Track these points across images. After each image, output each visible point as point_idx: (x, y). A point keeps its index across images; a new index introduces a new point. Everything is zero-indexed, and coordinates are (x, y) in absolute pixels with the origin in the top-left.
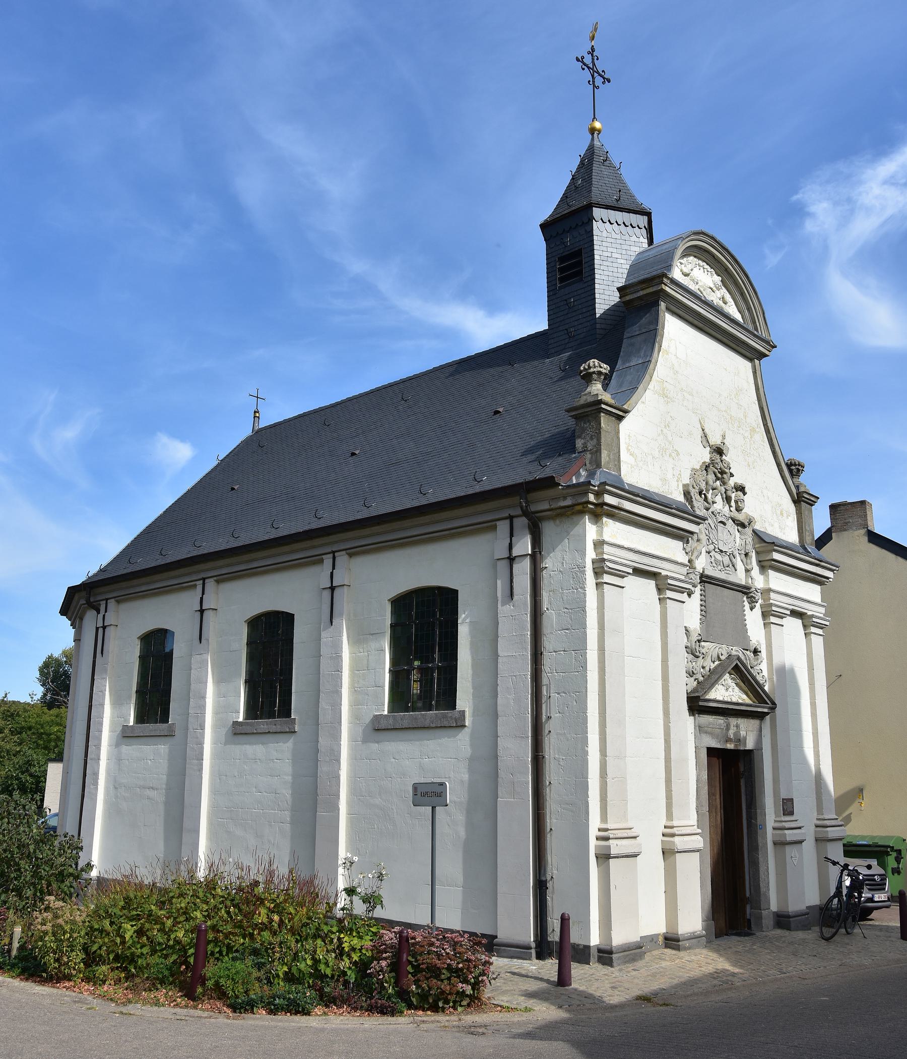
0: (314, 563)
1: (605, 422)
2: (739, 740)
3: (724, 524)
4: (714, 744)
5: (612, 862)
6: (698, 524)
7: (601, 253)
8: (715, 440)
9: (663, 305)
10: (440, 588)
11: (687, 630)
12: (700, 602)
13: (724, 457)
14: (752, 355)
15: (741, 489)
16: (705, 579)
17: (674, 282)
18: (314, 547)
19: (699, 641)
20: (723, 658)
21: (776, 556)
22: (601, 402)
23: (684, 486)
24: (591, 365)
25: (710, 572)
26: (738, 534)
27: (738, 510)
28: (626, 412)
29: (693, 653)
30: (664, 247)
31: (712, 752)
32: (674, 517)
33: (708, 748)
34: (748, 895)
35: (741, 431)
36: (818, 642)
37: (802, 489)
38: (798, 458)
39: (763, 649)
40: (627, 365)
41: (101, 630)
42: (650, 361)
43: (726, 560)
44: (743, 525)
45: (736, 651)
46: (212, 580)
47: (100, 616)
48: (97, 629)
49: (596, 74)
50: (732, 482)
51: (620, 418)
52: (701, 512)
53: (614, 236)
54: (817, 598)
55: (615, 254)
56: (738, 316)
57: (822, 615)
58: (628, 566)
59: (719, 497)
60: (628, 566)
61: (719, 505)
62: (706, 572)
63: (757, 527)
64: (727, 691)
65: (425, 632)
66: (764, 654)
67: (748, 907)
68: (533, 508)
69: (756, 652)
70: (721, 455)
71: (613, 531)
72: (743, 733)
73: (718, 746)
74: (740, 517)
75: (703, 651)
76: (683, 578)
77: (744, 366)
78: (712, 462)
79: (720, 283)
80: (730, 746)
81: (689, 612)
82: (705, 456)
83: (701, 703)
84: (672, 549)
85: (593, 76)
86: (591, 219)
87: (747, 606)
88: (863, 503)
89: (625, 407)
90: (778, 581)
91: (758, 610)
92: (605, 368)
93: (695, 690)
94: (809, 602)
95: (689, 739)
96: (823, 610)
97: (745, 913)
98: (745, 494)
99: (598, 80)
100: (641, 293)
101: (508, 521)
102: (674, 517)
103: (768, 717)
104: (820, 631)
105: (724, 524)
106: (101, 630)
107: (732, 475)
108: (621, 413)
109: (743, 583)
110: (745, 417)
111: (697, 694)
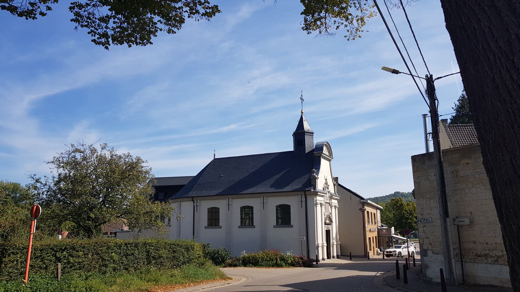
14: (330, 161)
64: (328, 221)
82: (325, 181)
90: (333, 201)
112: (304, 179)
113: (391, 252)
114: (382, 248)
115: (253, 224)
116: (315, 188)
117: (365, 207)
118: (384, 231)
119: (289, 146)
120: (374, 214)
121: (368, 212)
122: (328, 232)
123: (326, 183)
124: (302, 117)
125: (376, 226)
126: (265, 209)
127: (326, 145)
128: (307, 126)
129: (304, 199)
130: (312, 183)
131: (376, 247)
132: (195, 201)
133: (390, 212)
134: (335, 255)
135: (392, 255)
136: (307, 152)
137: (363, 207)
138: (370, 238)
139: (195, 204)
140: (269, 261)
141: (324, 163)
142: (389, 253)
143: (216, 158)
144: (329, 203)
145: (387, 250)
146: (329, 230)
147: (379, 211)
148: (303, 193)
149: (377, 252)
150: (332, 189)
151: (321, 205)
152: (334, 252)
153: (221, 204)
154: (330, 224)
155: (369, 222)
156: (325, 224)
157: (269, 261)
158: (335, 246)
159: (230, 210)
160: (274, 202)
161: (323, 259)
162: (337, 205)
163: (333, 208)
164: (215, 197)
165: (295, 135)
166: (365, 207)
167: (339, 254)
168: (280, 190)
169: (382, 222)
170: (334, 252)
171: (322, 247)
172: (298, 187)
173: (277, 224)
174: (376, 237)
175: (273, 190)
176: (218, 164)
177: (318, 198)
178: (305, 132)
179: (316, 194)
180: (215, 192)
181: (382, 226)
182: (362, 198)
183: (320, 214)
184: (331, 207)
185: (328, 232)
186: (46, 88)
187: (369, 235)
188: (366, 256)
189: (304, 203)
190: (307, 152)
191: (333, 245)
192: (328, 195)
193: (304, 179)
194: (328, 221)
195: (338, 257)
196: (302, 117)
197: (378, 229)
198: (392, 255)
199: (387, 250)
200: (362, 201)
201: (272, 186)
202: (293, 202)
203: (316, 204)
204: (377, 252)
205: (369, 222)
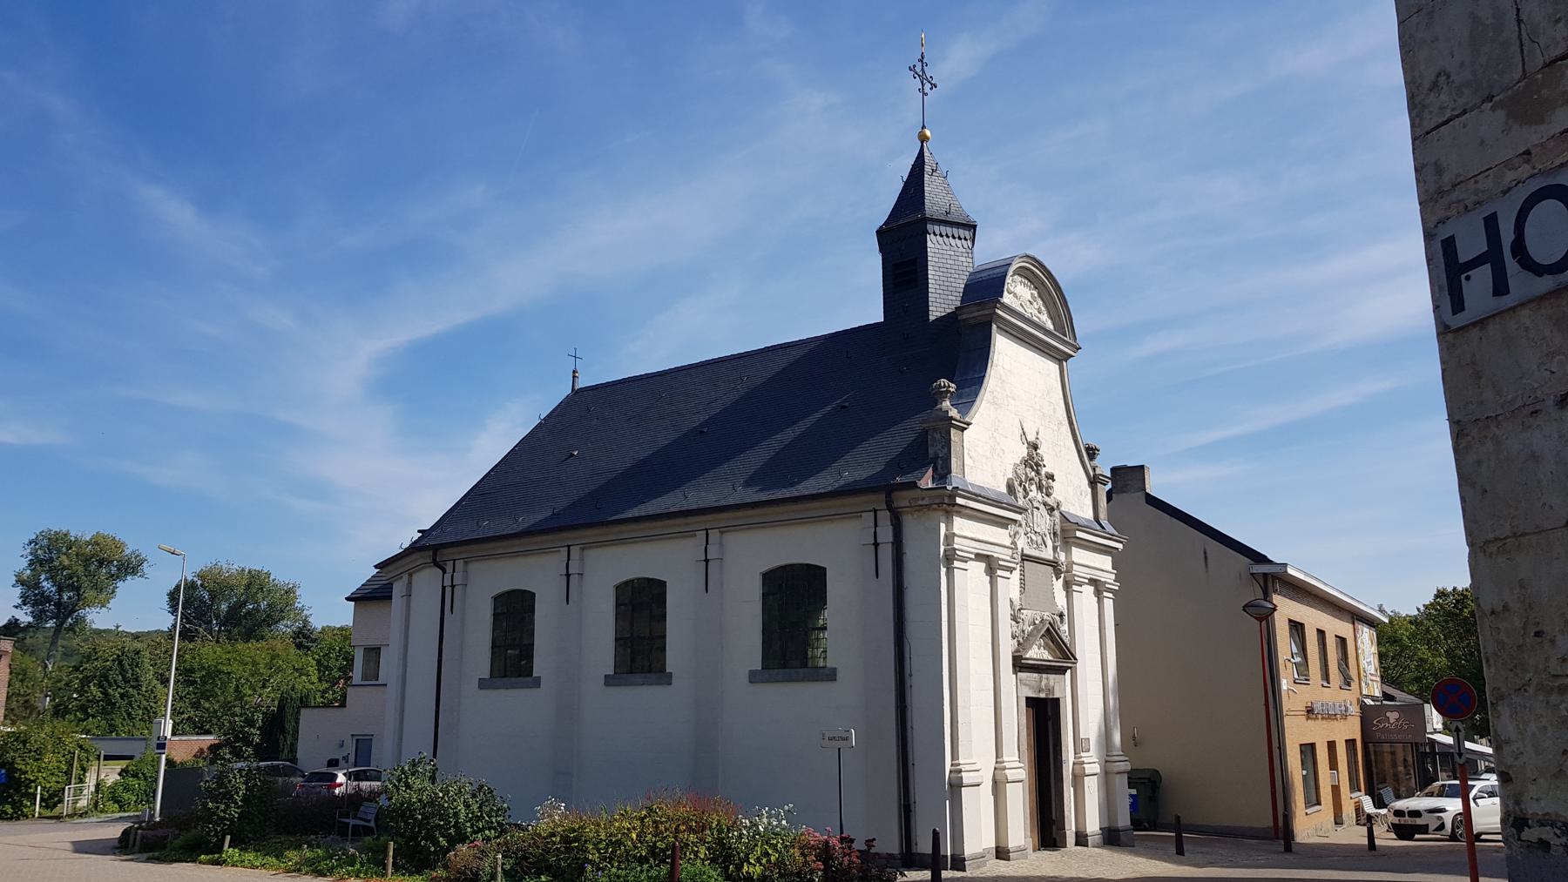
2: (1050, 690)
8: (1031, 438)
10: (808, 565)
14: (1061, 358)
15: (1051, 477)
16: (1025, 558)
17: (1105, 550)
21: (1079, 534)
27: (1048, 495)
29: (1015, 619)
32: (1002, 509)
36: (1109, 605)
37: (1098, 471)
38: (1093, 444)
41: (448, 590)
44: (1052, 509)
48: (444, 588)
55: (947, 272)
56: (1050, 325)
61: (1034, 493)
63: (1054, 484)
64: (1038, 652)
65: (794, 599)
69: (1061, 616)
74: (1050, 501)
77: (1053, 367)
78: (1030, 457)
80: (1042, 695)
81: (1010, 587)
82: (1023, 451)
84: (1001, 535)
90: (1078, 555)
99: (918, 69)
102: (1002, 509)
106: (448, 590)
112: (895, 440)
113: (1416, 814)
114: (1387, 793)
115: (663, 669)
117: (1277, 599)
118: (1393, 716)
119: (863, 305)
120: (1342, 641)
121: (1321, 633)
122: (1044, 718)
123: (1033, 461)
125: (1349, 698)
126: (716, 586)
127: (1022, 272)
128: (935, 196)
129: (886, 534)
130: (932, 449)
131: (1354, 787)
133: (1432, 643)
134: (1093, 825)
135: (1424, 829)
136: (932, 318)
137: (1267, 597)
138: (1308, 750)
139: (447, 583)
142: (1407, 820)
144: (1054, 565)
145: (1401, 804)
146: (1056, 702)
147: (1366, 636)
148: (879, 500)
149: (1359, 809)
150: (1074, 494)
151: (992, 566)
152: (1087, 807)
153: (536, 573)
154: (1062, 671)
155: (1302, 669)
156: (1020, 665)
157: (642, 860)
158: (1092, 787)
161: (1002, 853)
162: (1109, 578)
164: (517, 545)
165: (886, 236)
166: (1277, 599)
167: (1124, 820)
169: (1386, 678)
170: (1087, 807)
171: (998, 786)
172: (861, 474)
174: (1350, 743)
175: (752, 495)
176: (587, 411)
177: (961, 525)
178: (926, 220)
179: (947, 503)
180: (524, 522)
181: (1387, 696)
182: (1261, 559)
183: (976, 620)
184: (1067, 586)
185: (1044, 718)
186: (415, 318)
187: (1297, 732)
188: (1282, 832)
189: (886, 553)
190: (932, 318)
191: (1078, 779)
192: (1043, 522)
193: (895, 440)
194: (1038, 652)
195: (1112, 838)
197: (1363, 706)
198: (1424, 829)
199: (1401, 804)
200: (1261, 569)
201: (748, 483)
202: (836, 547)
203: (951, 557)
204: (1359, 809)
205: (1302, 669)
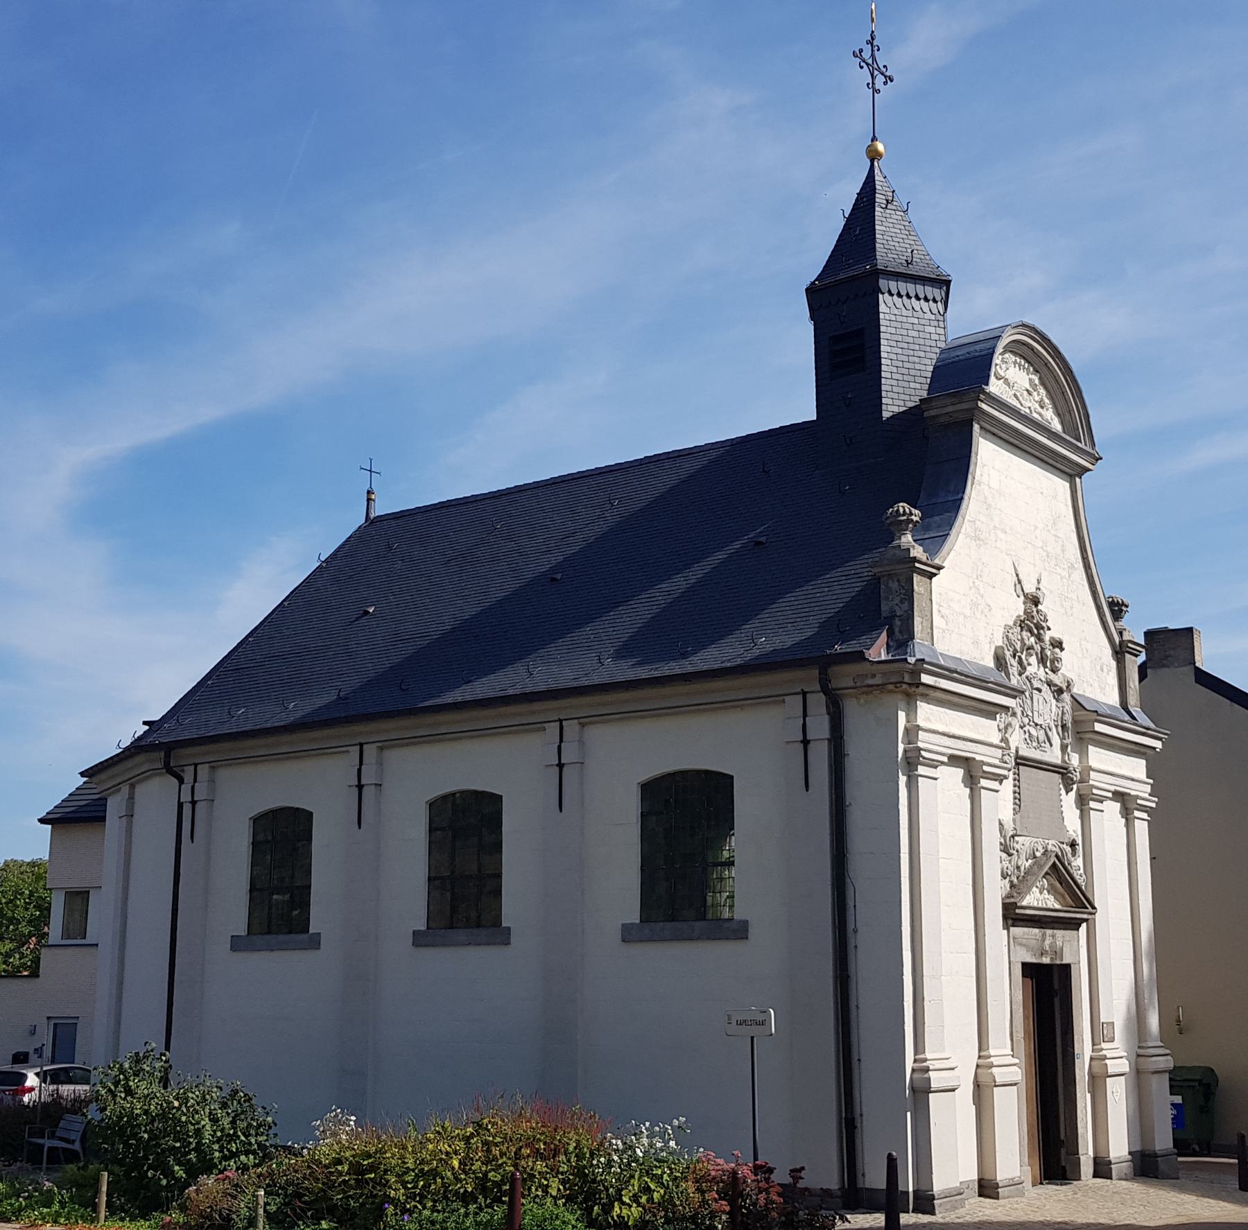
0: (538, 730)
1: (918, 582)
3: (1039, 690)
4: (1030, 959)
5: (931, 1095)
6: (1015, 697)
7: (888, 336)
8: (1030, 588)
9: (976, 427)
11: (1000, 824)
12: (1012, 788)
13: (1040, 607)
14: (1073, 473)
15: (1058, 644)
16: (1021, 761)
18: (533, 713)
19: (1013, 836)
20: (1038, 854)
21: (1099, 727)
22: (915, 560)
23: (997, 648)
24: (901, 510)
25: (1024, 752)
26: (1054, 702)
28: (939, 568)
29: (1006, 849)
30: (977, 347)
31: (1028, 969)
32: (987, 690)
33: (1024, 964)
34: (1062, 1137)
35: (1059, 571)
36: (1142, 829)
37: (1126, 637)
38: (1119, 597)
39: (1079, 841)
40: (933, 501)
42: (962, 498)
43: (1042, 737)
44: (1060, 691)
45: (1052, 845)
46: (374, 746)
47: (186, 788)
48: (180, 805)
49: (876, 72)
50: (1047, 636)
51: (931, 576)
52: (1015, 681)
53: (905, 312)
54: (1141, 773)
56: (1056, 426)
57: (1146, 796)
58: (944, 755)
59: (1034, 657)
60: (944, 755)
61: (1034, 668)
62: (1021, 753)
64: (1038, 898)
65: (686, 823)
66: (1080, 848)
67: (1063, 1151)
68: (833, 685)
69: (1073, 845)
70: (1036, 606)
71: (928, 714)
72: (1059, 943)
73: (1034, 960)
74: (1057, 679)
75: (1017, 846)
76: (997, 762)
77: (1062, 486)
79: (1037, 382)
80: (1046, 960)
81: (999, 803)
82: (1018, 608)
83: (1018, 911)
84: (987, 729)
85: (872, 75)
86: (879, 291)
87: (1063, 792)
88: (1190, 630)
89: (937, 561)
90: (1098, 757)
91: (1073, 794)
92: (916, 515)
93: (1009, 896)
94: (1133, 780)
95: (1005, 953)
96: (1148, 788)
97: (1059, 1160)
98: (1062, 649)
100: (951, 409)
101: (800, 697)
102: (987, 690)
103: (1084, 925)
104: (1145, 816)
105: (1039, 690)
106: (187, 809)
107: (1049, 629)
108: (934, 571)
109: (1059, 762)
110: (1063, 551)
111: (1012, 900)
112: (834, 591)
116: (902, 638)
119: (786, 396)
122: (1048, 991)
124: (870, 182)
127: (1016, 348)
129: (820, 727)
130: (886, 606)
132: (188, 776)
134: (1119, 1148)
139: (186, 797)
140: (466, 1199)
141: (1000, 480)
143: (379, 510)
144: (1063, 771)
146: (1065, 971)
148: (809, 678)
150: (1092, 671)
151: (972, 772)
152: (1111, 1120)
153: (314, 782)
154: (1074, 925)
156: (1013, 916)
157: (466, 1199)
159: (372, 824)
160: (630, 754)
161: (987, 1188)
162: (1142, 791)
163: (1108, 817)
167: (1163, 1140)
168: (675, 668)
170: (1111, 1120)
171: (982, 1092)
172: (784, 640)
173: (646, 917)
175: (627, 671)
176: (388, 547)
178: (877, 273)
179: (907, 681)
180: (297, 708)
184: (1082, 802)
185: (1048, 991)
191: (1098, 1081)
192: (1047, 709)
193: (834, 591)
195: (1146, 1166)
196: (870, 182)
201: (619, 655)
202: (749, 745)
203: (913, 760)
